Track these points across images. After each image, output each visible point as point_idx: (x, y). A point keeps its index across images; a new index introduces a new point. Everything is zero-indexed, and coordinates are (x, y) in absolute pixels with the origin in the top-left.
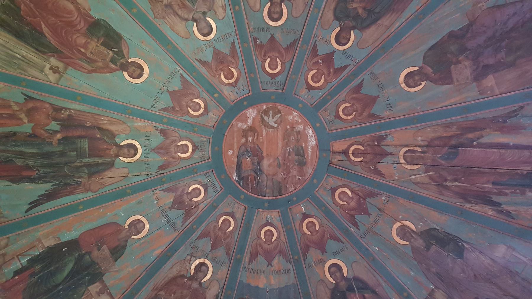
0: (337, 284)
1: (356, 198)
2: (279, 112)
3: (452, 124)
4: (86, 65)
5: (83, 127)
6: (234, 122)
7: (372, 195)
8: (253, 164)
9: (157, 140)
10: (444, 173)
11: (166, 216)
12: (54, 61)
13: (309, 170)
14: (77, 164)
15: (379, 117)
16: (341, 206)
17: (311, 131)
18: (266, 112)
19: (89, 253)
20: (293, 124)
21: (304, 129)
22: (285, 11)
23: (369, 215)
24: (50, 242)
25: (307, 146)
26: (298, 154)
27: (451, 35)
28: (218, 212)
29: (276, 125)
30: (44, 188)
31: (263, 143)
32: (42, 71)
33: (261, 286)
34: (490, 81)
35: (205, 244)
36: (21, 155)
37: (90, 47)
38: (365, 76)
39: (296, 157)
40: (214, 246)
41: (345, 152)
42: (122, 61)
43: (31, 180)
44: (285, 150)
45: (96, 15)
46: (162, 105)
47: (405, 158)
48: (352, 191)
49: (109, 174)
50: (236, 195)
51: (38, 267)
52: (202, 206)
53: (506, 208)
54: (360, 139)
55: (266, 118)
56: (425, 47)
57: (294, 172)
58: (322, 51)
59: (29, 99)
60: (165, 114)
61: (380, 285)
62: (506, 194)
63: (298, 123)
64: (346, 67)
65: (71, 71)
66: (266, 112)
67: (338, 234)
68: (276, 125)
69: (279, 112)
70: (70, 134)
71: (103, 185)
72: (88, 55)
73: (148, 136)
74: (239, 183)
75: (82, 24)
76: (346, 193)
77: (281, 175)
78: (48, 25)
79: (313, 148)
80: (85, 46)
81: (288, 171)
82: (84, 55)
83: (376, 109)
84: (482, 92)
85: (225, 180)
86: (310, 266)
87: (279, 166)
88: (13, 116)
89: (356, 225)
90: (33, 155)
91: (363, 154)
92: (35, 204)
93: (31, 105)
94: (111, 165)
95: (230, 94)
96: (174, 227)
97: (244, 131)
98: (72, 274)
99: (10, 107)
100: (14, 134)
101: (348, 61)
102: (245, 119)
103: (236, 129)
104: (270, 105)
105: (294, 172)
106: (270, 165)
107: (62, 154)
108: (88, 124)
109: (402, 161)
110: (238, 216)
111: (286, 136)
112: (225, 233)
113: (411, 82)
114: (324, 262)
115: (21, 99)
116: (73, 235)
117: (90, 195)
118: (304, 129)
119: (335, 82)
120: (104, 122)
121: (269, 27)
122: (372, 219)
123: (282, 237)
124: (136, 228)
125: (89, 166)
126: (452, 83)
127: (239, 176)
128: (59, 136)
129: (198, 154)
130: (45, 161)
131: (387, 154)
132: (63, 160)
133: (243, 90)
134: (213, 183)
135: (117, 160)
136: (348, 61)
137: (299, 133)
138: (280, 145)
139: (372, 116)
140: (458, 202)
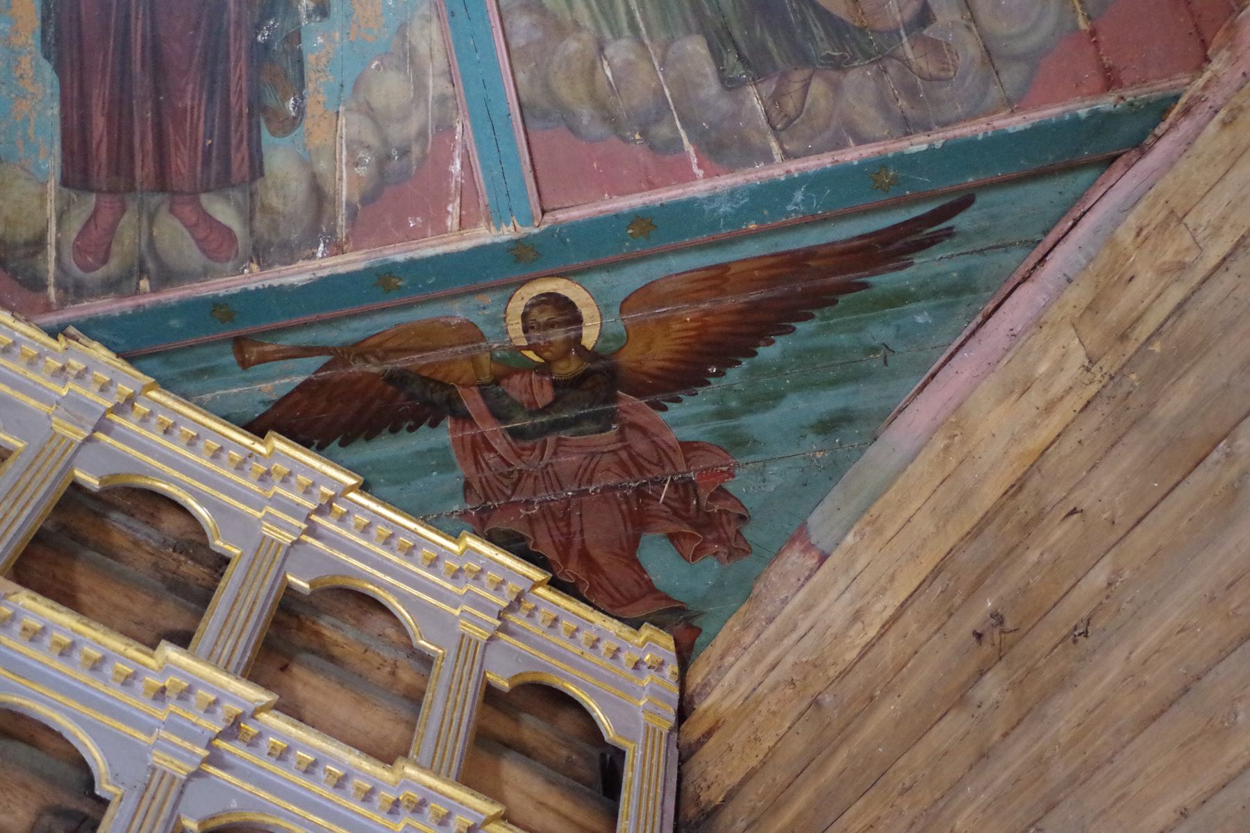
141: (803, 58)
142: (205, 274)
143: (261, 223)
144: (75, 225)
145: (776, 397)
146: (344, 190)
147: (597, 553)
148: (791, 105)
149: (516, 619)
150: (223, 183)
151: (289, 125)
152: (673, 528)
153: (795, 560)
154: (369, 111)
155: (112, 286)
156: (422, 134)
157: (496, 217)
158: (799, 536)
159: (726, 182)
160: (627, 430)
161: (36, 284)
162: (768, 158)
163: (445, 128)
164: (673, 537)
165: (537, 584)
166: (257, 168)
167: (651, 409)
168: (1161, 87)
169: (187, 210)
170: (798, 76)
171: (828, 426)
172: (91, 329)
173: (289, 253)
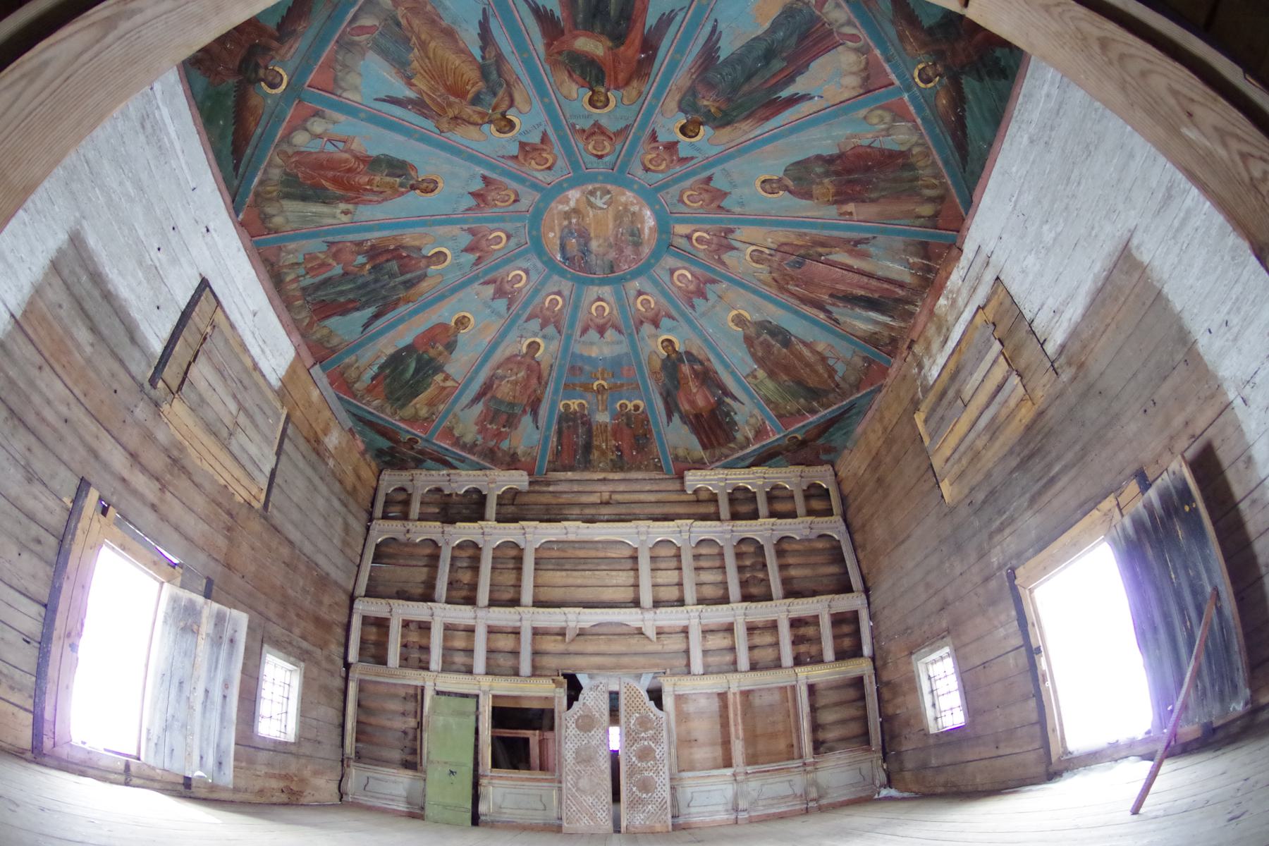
0: (668, 356)
1: (695, 282)
2: (609, 192)
3: (805, 234)
4: (375, 198)
5: (388, 251)
6: (553, 205)
7: (713, 281)
8: (579, 244)
9: (466, 239)
11: (490, 307)
12: (343, 206)
13: (646, 250)
14: (392, 284)
16: (679, 288)
17: (648, 213)
18: (592, 193)
20: (626, 205)
21: (640, 209)
23: (707, 300)
24: (390, 351)
25: (643, 229)
26: (632, 234)
28: (543, 293)
29: (605, 206)
30: (369, 312)
31: (590, 224)
32: (334, 217)
33: (593, 355)
35: (535, 324)
36: (342, 293)
37: (375, 182)
38: (716, 171)
39: (631, 238)
40: (543, 326)
41: (689, 237)
42: (411, 182)
43: (357, 309)
44: (618, 231)
47: (751, 257)
48: (692, 275)
50: (562, 274)
51: (388, 371)
52: (524, 291)
54: (708, 227)
55: (592, 199)
57: (629, 251)
59: (331, 244)
61: (709, 360)
62: (838, 306)
63: (632, 204)
64: (692, 158)
65: (361, 208)
66: (592, 193)
67: (674, 313)
68: (605, 206)
69: (609, 192)
70: (378, 261)
72: (375, 189)
74: (564, 263)
75: (362, 166)
76: (686, 276)
77: (612, 255)
78: (327, 179)
79: (650, 229)
81: (621, 251)
82: (371, 190)
85: (550, 263)
86: (643, 339)
87: (610, 246)
88: (323, 265)
89: (693, 307)
90: (351, 290)
91: (708, 243)
92: (366, 326)
93: (334, 249)
94: (423, 277)
96: (499, 315)
97: (566, 213)
98: (417, 371)
99: (317, 258)
100: (330, 278)
101: (695, 153)
102: (567, 201)
103: (555, 212)
104: (597, 185)
106: (599, 246)
107: (376, 281)
108: (392, 247)
109: (748, 257)
110: (566, 293)
111: (618, 217)
112: (554, 312)
114: (657, 337)
115: (324, 247)
116: (407, 340)
118: (640, 209)
122: (710, 303)
123: (615, 312)
124: (463, 324)
125: (405, 283)
127: (564, 256)
128: (368, 267)
129: (513, 241)
131: (733, 248)
132: (378, 285)
134: (535, 266)
137: (634, 213)
138: (611, 226)
149: (692, 529)
150: (730, 442)
153: (846, 452)
157: (779, 433)
158: (845, 447)
161: (705, 464)
166: (735, 438)
167: (964, 261)
168: (879, 384)
171: (844, 434)
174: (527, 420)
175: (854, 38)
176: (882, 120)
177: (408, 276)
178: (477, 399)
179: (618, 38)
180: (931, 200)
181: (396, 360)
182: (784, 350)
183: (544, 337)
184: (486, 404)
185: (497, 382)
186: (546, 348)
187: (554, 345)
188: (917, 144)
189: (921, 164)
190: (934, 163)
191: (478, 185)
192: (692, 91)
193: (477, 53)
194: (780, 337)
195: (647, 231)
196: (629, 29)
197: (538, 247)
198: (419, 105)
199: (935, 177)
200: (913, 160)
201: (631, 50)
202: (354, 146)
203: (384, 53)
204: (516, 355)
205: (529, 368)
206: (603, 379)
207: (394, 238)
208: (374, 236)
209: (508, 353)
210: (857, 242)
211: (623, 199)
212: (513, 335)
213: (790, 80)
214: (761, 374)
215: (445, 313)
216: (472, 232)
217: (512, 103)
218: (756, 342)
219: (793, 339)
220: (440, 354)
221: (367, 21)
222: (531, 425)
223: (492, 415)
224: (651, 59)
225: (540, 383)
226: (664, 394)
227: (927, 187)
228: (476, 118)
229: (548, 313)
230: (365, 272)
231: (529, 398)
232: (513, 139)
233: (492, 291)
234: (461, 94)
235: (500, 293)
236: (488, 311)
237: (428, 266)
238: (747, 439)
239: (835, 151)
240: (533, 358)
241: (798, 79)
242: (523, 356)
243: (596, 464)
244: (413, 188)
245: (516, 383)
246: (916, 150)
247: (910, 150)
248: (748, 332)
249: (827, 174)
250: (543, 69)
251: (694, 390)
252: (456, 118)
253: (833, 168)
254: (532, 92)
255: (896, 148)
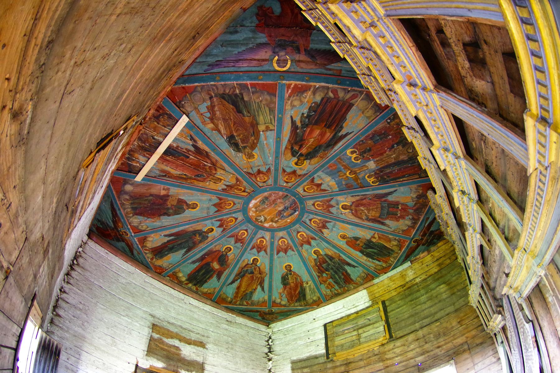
5: (319, 268)
10: (208, 170)
13: (266, 194)
15: (218, 198)
18: (261, 222)
19: (362, 247)
22: (224, 248)
24: (365, 258)
26: (264, 202)
27: (169, 215)
30: (347, 268)
34: (163, 193)
36: (340, 277)
40: (332, 206)
43: (346, 272)
45: (282, 286)
46: (293, 253)
49: (330, 254)
53: (191, 143)
55: (263, 221)
56: (182, 215)
58: (221, 229)
59: (321, 283)
60: (295, 249)
62: (186, 149)
63: (253, 211)
65: (304, 280)
71: (335, 253)
73: (307, 250)
78: (295, 292)
79: (256, 200)
80: (293, 282)
81: (274, 201)
83: (217, 201)
84: (168, 189)
87: (276, 204)
90: (338, 275)
92: (354, 266)
94: (326, 255)
95: (267, 235)
101: (214, 222)
105: (273, 198)
107: (332, 269)
113: (195, 206)
117: (341, 255)
119: (225, 217)
120: (313, 263)
121: (234, 247)
125: (331, 260)
126: (179, 199)
129: (300, 230)
130: (338, 272)
133: (261, 233)
135: (323, 254)
136: (214, 222)
139: (220, 199)
140: (212, 154)
141: (229, 95)
142: (338, 88)
143: (326, 92)
144: (355, 100)
145: (245, 39)
146: (310, 93)
147: (290, 14)
148: (232, 90)
150: (329, 99)
151: (315, 103)
152: (272, 15)
154: (301, 101)
155: (354, 90)
156: (294, 96)
159: (244, 82)
160: (60, 300)
162: (237, 84)
163: (290, 96)
164: (273, 13)
165: (304, 11)
166: (322, 99)
169: (337, 96)
170: (231, 93)
172: (362, 87)
173: (323, 87)
174: (390, 198)
175: (146, 250)
176: (142, 227)
177: (327, 260)
178: (383, 224)
179: (208, 264)
180: (126, 193)
181: (368, 255)
182: (235, 134)
183: (338, 204)
184: (386, 219)
185: (370, 217)
186: (343, 202)
187: (339, 198)
188: (131, 217)
189: (129, 210)
190: (124, 209)
191: (282, 254)
192: (201, 242)
193: (239, 281)
194: (233, 141)
195: (258, 200)
196: (204, 265)
197: (298, 221)
198: (261, 284)
199: (124, 204)
200: (133, 212)
201: (208, 259)
202: (281, 291)
203: (251, 297)
204: (352, 213)
205: (357, 206)
206: (345, 174)
207: (313, 267)
208: (315, 274)
209: (353, 217)
210: (165, 176)
211: (254, 214)
212: (343, 217)
213: (168, 241)
214: (261, 128)
215: (342, 243)
216: (302, 245)
217: (248, 264)
218: (249, 145)
219: (225, 138)
220: (361, 242)
221: (245, 303)
222: (394, 195)
223: (393, 216)
224: (205, 255)
225: (365, 199)
226: (331, 147)
227: (127, 200)
228: (258, 269)
229: (325, 207)
230: (329, 273)
231: (376, 201)
232: (259, 256)
233: (325, 230)
234: (252, 277)
235: (324, 227)
236: (334, 229)
237: (321, 255)
238: (314, 93)
239: (162, 217)
240: (351, 206)
241: (166, 241)
242: (352, 210)
243: (411, 155)
244: (291, 271)
245: (369, 210)
246: (131, 215)
247: (133, 215)
248: (250, 151)
249: (168, 209)
250: (232, 267)
251: (313, 139)
252: (260, 274)
253: (165, 211)
254: (240, 262)
255: (139, 217)
